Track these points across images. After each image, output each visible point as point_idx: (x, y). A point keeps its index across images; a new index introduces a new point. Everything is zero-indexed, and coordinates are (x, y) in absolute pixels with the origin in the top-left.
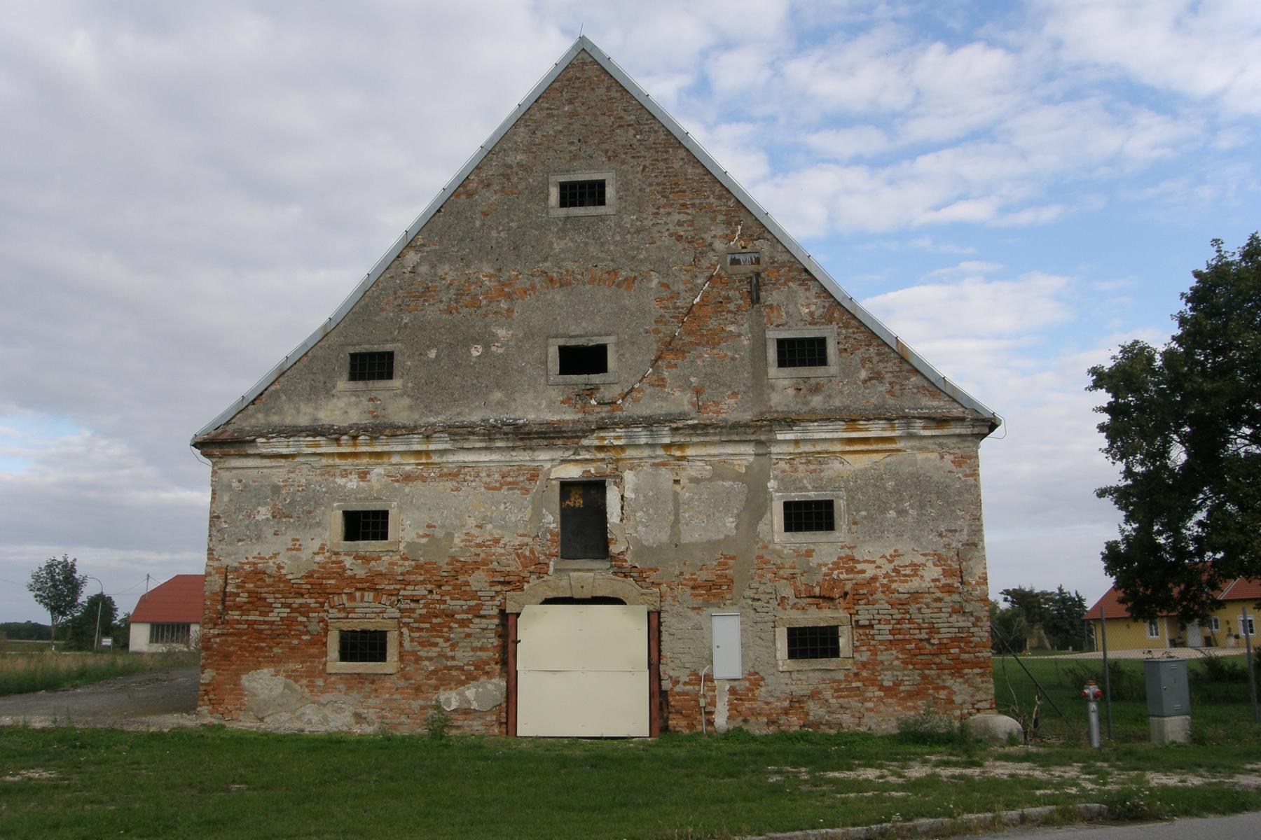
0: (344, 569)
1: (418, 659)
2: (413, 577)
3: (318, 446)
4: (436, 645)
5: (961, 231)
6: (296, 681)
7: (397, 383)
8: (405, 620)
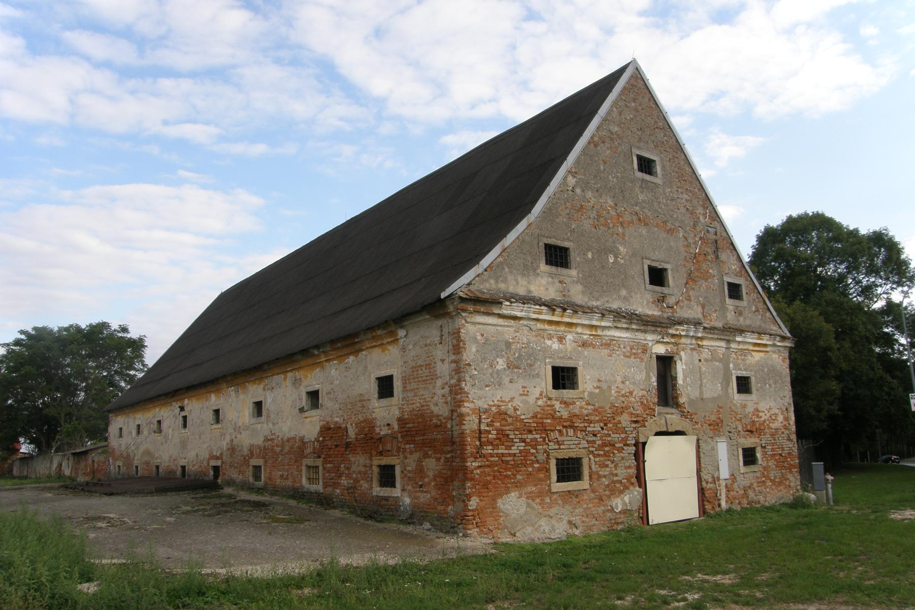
0: (555, 411)
1: (600, 477)
2: (592, 418)
3: (540, 313)
4: (607, 466)
5: (183, 146)
6: (533, 501)
7: (573, 272)
8: (591, 449)
